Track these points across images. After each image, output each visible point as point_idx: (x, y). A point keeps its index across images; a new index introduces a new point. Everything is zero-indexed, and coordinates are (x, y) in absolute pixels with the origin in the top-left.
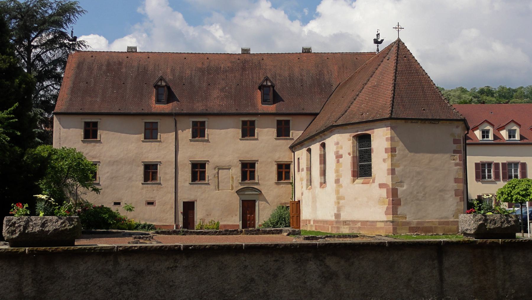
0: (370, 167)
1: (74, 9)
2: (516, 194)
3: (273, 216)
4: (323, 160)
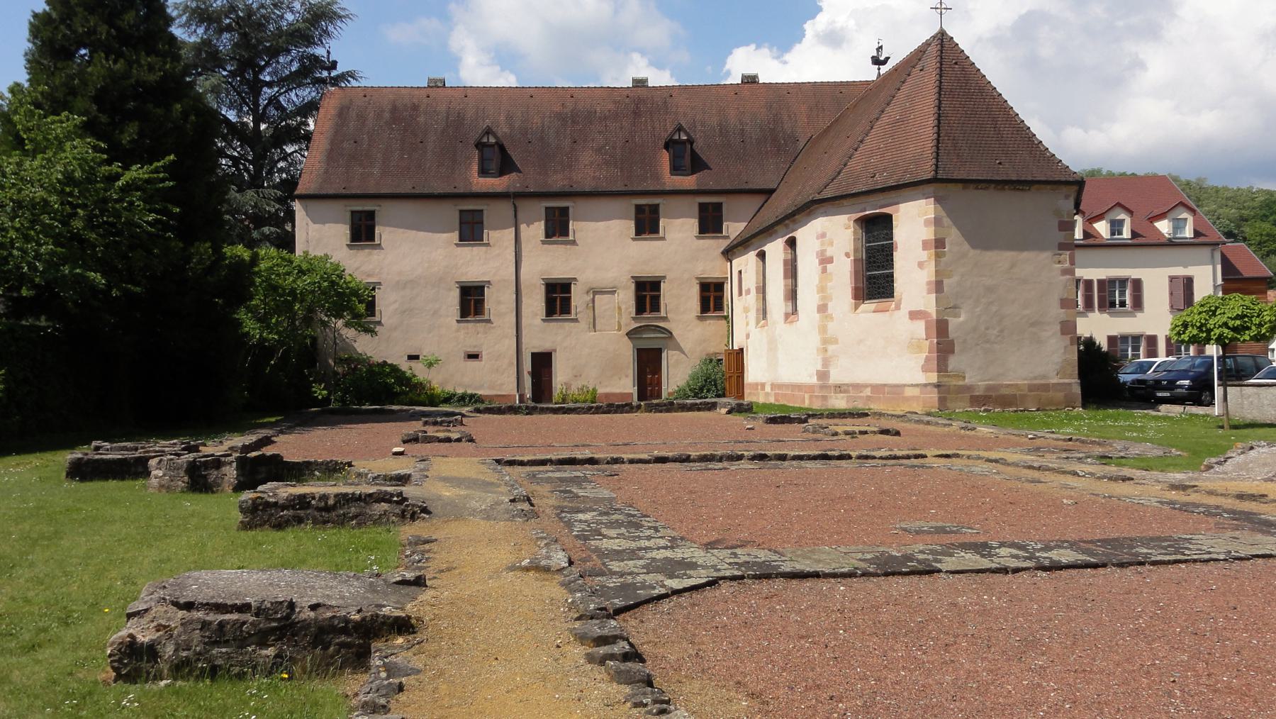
0: (890, 278)
1: (335, 13)
2: (1220, 326)
3: (694, 377)
4: (791, 270)
